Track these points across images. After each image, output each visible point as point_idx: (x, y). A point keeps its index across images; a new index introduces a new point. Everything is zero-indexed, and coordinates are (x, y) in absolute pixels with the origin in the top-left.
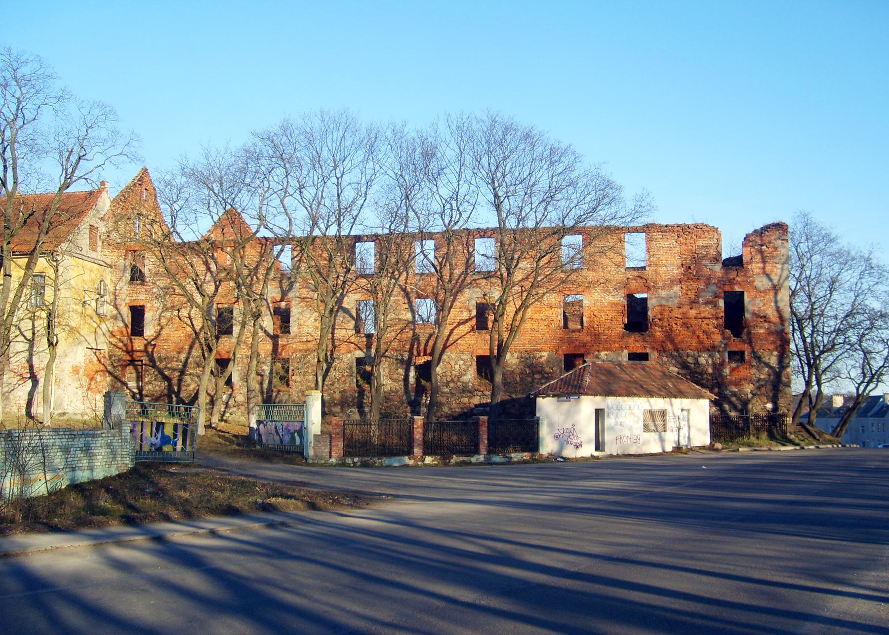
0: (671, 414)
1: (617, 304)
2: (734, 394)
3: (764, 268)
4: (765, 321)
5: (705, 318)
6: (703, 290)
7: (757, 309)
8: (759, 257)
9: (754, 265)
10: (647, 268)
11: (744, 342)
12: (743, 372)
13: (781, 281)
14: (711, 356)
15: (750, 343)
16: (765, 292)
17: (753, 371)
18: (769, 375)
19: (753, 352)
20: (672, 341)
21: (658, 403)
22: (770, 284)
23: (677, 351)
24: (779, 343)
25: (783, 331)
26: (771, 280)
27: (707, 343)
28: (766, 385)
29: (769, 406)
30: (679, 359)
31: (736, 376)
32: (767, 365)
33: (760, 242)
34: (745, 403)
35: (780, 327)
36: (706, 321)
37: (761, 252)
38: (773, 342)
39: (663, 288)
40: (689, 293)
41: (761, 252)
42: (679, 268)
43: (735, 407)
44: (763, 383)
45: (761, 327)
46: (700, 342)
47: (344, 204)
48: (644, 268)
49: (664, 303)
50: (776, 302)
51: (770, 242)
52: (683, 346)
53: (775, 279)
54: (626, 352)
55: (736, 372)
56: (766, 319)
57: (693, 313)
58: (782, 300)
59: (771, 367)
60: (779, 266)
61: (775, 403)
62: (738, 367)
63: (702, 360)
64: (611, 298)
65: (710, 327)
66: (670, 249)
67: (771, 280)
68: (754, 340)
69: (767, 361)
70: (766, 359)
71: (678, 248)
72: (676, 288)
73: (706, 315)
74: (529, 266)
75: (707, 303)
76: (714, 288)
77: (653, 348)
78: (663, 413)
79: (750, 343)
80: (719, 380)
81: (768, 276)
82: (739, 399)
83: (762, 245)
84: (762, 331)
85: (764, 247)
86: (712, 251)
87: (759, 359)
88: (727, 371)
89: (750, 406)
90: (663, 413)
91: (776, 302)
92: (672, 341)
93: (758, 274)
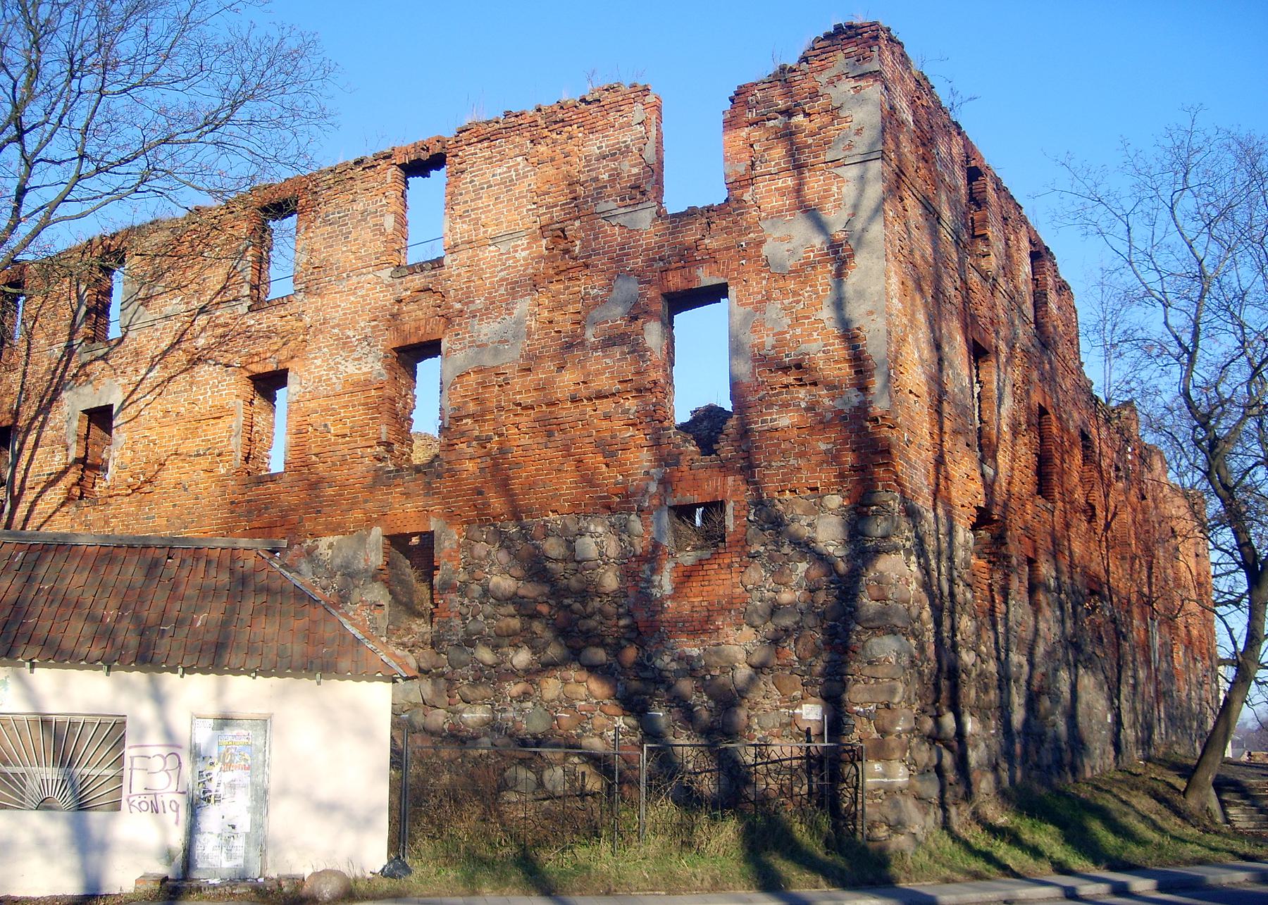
0: (154, 739)
1: (365, 385)
2: (690, 668)
3: (798, 190)
4: (801, 383)
5: (600, 396)
6: (598, 302)
7: (769, 341)
8: (779, 153)
9: (762, 186)
10: (447, 261)
11: (725, 468)
12: (723, 582)
13: (858, 226)
14: (621, 530)
15: (748, 470)
16: (801, 272)
17: (756, 574)
18: (812, 591)
19: (759, 503)
20: (504, 486)
21: (79, 692)
22: (818, 241)
23: (516, 515)
24: (849, 458)
25: (862, 412)
26: (821, 226)
27: (610, 477)
28: (799, 628)
29: (811, 712)
30: (519, 545)
31: (696, 600)
32: (806, 548)
33: (782, 104)
34: (728, 700)
35: (854, 397)
36: (606, 406)
37: (788, 135)
38: (833, 458)
39: (485, 313)
40: (557, 316)
41: (788, 135)
42: (534, 240)
43: (688, 715)
44: (787, 621)
45: (785, 406)
46: (588, 480)
47: (989, 481)
48: (438, 263)
49: (488, 361)
50: (839, 304)
51: (814, 95)
52: (531, 500)
53: (836, 219)
54: (377, 532)
55: (695, 585)
56: (800, 369)
57: (567, 381)
58: (860, 294)
59: (821, 558)
60: (852, 172)
61: (835, 703)
62: (701, 562)
63: (588, 547)
64: (351, 368)
65: (617, 424)
66: (508, 184)
67: (821, 226)
68: (761, 458)
69: (806, 532)
70: (801, 528)
71: (531, 178)
72: (523, 306)
73: (605, 383)
74: (183, 307)
75: (609, 342)
76: (631, 287)
77: (450, 517)
78: (115, 733)
79: (748, 470)
80: (641, 615)
81: (813, 214)
82: (705, 685)
83: (788, 113)
84: (785, 420)
85: (799, 119)
86: (626, 166)
87: (775, 524)
88: (665, 582)
89: (742, 714)
90: (115, 733)
91: (839, 304)
92: (504, 486)
93: (777, 214)
